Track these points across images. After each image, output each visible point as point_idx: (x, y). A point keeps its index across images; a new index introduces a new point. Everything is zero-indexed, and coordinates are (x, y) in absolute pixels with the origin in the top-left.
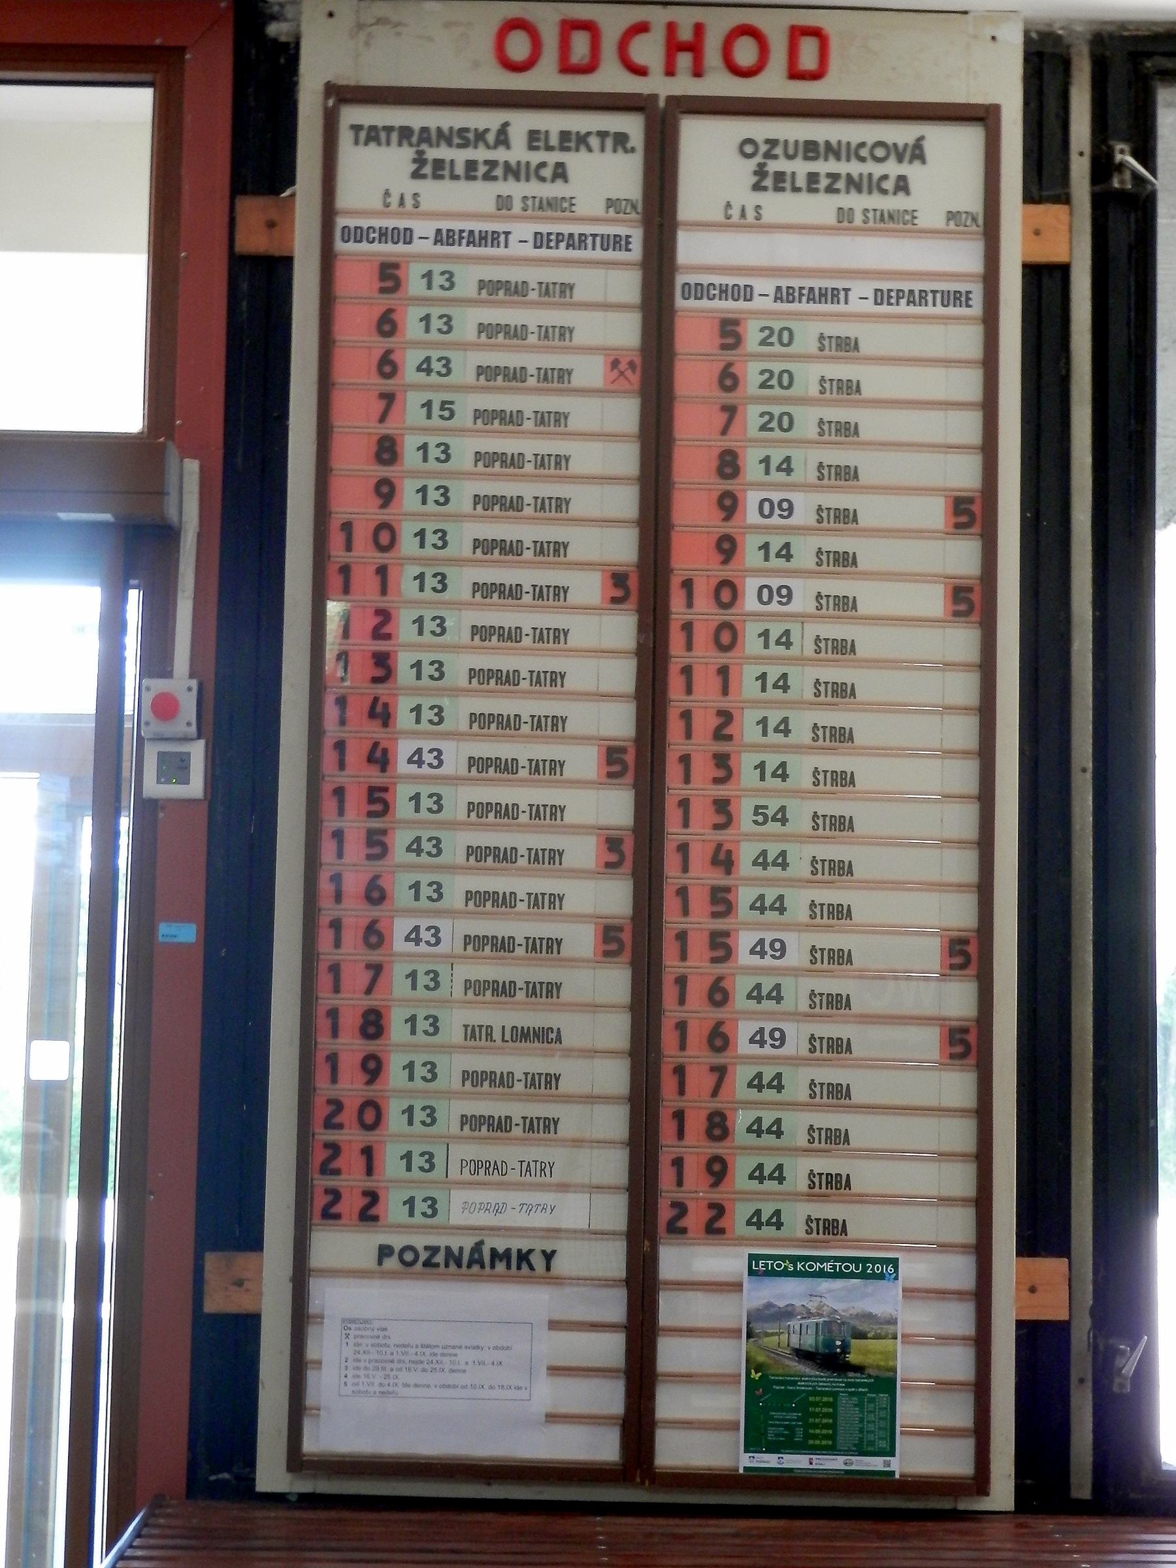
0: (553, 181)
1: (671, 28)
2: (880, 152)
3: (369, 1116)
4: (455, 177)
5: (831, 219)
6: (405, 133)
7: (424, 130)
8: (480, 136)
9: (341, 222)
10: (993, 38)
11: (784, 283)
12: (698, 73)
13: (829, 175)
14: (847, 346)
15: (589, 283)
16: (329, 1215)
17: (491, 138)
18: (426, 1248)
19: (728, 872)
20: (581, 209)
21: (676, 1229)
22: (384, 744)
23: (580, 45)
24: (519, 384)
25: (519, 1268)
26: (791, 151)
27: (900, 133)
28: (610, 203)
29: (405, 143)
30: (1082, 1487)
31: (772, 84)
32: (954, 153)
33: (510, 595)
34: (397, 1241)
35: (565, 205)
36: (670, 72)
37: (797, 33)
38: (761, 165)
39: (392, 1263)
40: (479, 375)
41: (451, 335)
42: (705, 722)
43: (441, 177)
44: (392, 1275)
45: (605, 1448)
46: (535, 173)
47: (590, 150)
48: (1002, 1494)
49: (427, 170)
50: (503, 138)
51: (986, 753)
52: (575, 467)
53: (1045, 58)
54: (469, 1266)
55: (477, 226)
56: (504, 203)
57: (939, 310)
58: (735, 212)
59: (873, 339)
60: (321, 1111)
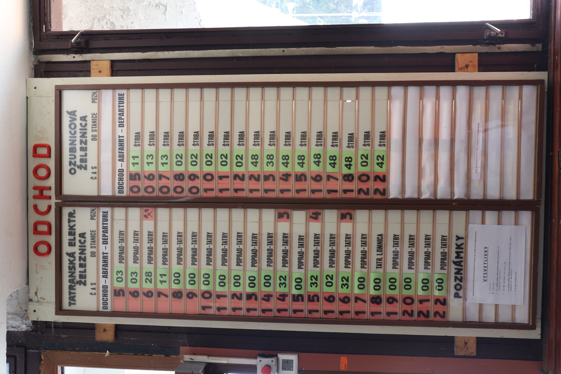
0: (85, 238)
1: (35, 197)
2: (73, 126)
3: (409, 301)
4: (85, 271)
5: (95, 142)
6: (71, 288)
7: (70, 281)
8: (71, 262)
9: (101, 309)
10: (35, 88)
11: (117, 158)
12: (50, 188)
13: (81, 144)
14: (138, 136)
15: (119, 226)
16: (444, 315)
17: (72, 259)
18: (455, 281)
19: (290, 175)
20: (95, 228)
21: (384, 192)
22: (278, 296)
23: (44, 228)
24: (168, 250)
25: (462, 248)
26: (73, 157)
27: (66, 119)
28: (92, 218)
29: (74, 288)
30: (539, 47)
31: (51, 163)
32: (71, 100)
33: (286, 254)
34: (453, 291)
35: (93, 233)
36: (49, 198)
37: (35, 155)
38: (78, 167)
39: (461, 293)
40: (151, 263)
41: (137, 272)
42: (253, 185)
43: (85, 275)
44: (465, 294)
45: (526, 217)
46: (83, 244)
47: (75, 225)
48: (542, 75)
49: (83, 280)
50: (72, 255)
51: (373, 84)
52: (152, 230)
53: (42, 70)
54: (462, 266)
55: (101, 263)
56: (93, 254)
57: (125, 105)
58: (94, 176)
59: (135, 128)
60: (407, 317)
